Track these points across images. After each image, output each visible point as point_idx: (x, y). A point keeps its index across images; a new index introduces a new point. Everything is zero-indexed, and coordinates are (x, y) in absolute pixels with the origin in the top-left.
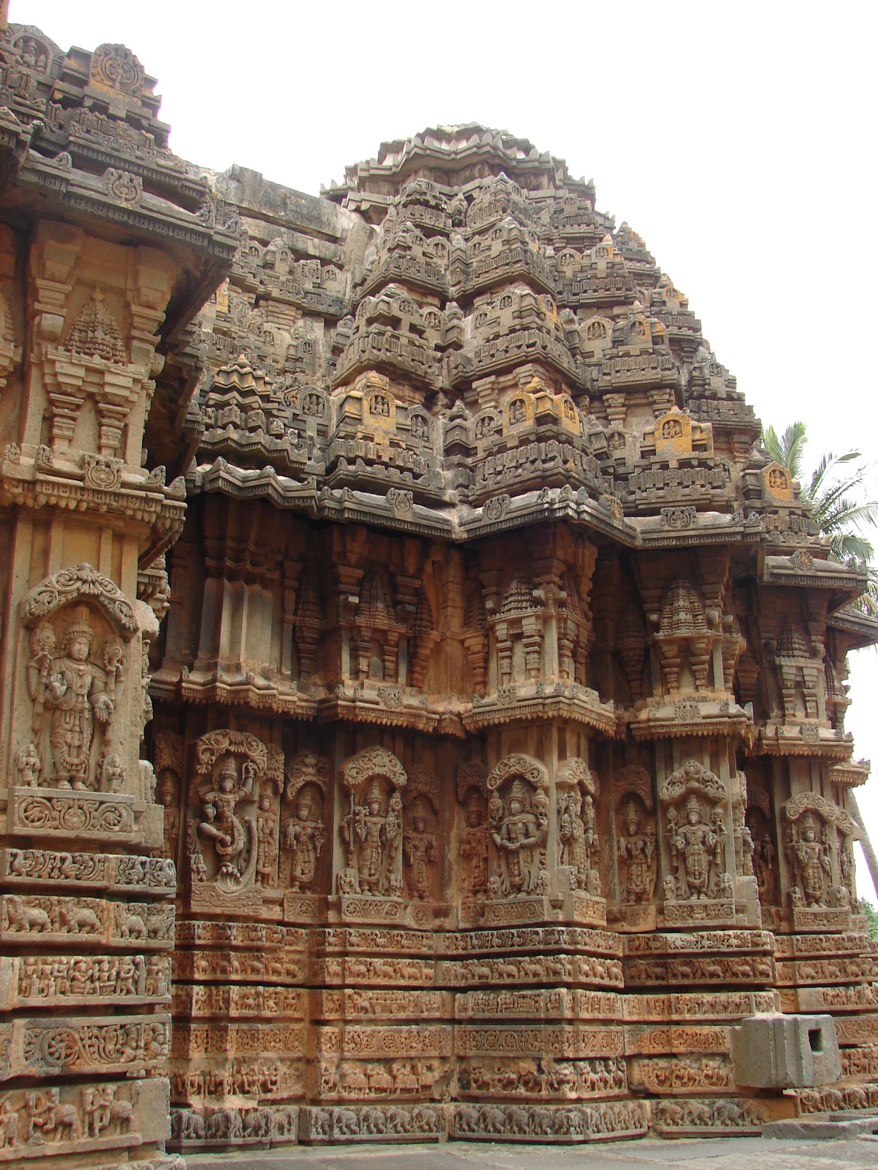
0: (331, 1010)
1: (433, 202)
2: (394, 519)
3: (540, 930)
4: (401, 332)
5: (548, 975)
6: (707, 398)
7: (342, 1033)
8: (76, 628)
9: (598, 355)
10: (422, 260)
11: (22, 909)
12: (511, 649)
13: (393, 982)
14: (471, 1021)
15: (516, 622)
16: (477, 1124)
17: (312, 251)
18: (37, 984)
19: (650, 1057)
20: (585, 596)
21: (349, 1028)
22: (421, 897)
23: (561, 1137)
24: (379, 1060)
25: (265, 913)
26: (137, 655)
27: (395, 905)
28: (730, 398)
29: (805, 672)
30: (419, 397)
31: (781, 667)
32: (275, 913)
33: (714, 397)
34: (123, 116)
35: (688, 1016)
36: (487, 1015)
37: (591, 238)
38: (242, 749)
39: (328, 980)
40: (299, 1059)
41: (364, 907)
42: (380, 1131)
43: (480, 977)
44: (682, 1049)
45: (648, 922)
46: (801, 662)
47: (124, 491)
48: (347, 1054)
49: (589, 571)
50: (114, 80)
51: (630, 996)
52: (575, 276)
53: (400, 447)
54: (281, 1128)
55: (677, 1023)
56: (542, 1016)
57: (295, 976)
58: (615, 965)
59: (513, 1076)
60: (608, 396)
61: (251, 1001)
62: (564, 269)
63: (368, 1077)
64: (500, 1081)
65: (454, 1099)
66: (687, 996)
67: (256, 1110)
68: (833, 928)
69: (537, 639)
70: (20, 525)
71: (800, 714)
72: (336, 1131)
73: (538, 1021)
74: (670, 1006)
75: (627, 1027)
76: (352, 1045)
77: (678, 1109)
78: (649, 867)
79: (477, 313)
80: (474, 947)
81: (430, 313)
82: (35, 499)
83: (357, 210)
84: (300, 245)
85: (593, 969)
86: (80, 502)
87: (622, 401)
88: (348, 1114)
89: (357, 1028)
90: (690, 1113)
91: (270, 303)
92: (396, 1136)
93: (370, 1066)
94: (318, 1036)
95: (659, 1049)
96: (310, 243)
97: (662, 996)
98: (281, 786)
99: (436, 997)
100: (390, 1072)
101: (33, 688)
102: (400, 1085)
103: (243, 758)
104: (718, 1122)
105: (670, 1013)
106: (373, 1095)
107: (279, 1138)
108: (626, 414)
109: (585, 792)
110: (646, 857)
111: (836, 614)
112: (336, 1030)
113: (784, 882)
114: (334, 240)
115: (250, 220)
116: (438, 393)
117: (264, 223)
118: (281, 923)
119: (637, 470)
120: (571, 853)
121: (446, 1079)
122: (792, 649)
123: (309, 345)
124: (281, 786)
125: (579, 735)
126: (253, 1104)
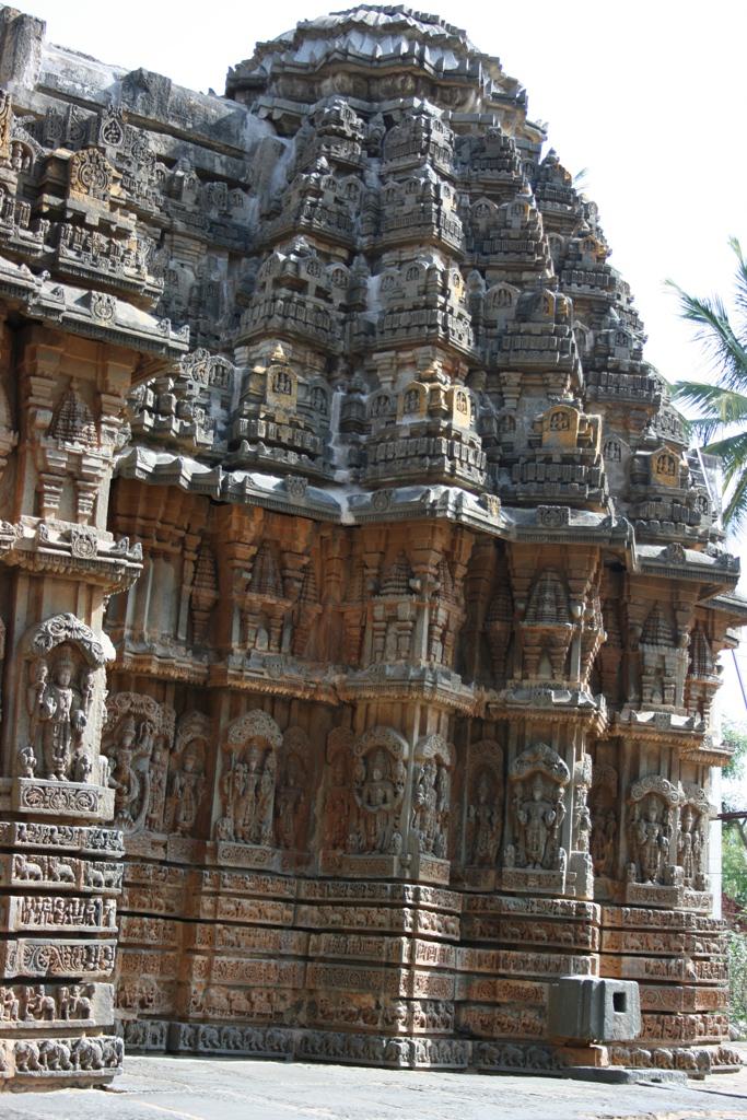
0: (202, 942)
1: (349, 134)
2: (287, 505)
3: (389, 885)
4: (308, 297)
5: (391, 925)
6: (608, 370)
7: (211, 962)
8: (63, 663)
9: (501, 326)
10: (334, 207)
11: (25, 863)
12: (386, 630)
13: (258, 921)
14: (323, 960)
15: (392, 607)
16: (320, 1047)
17: (219, 170)
18: (33, 916)
19: (477, 1003)
20: (458, 582)
21: (217, 958)
22: (287, 847)
23: (388, 1063)
24: (240, 987)
25: (150, 854)
26: (98, 679)
27: (264, 853)
28: (632, 370)
29: (667, 660)
30: (320, 363)
31: (643, 654)
32: (160, 854)
33: (617, 370)
34: (97, 224)
35: (513, 972)
36: (336, 956)
37: (510, 186)
38: (142, 711)
39: (202, 917)
40: (171, 982)
41: (238, 854)
42: (237, 1048)
43: (333, 922)
44: (505, 1000)
45: (488, 883)
46: (664, 650)
47: (99, 558)
48: (215, 981)
49: (465, 559)
50: (88, 188)
51: (464, 950)
52: (488, 231)
53: (299, 427)
54: (154, 1040)
55: (503, 976)
56: (384, 959)
57: (172, 910)
58: (453, 921)
59: (355, 1010)
60: (504, 374)
61: (137, 930)
62: (479, 221)
63: (230, 1001)
64: (343, 1013)
65: (303, 1026)
66: (514, 953)
67: (135, 1022)
68: (663, 905)
69: (411, 624)
70: (20, 580)
71: (658, 699)
72: (201, 1044)
73: (381, 964)
74: (498, 962)
75: (458, 976)
76: (219, 973)
77: (496, 1051)
78: (493, 834)
79: (383, 274)
80: (329, 896)
81: (337, 271)
82: (35, 565)
83: (269, 118)
84: (207, 165)
85: (432, 923)
86: (67, 568)
87: (518, 380)
88: (212, 1033)
89: (224, 958)
90: (506, 1055)
91: (176, 237)
92: (251, 1053)
93: (232, 992)
94: (191, 961)
95: (485, 998)
96: (217, 161)
97: (493, 952)
98: (172, 742)
99: (295, 937)
100: (249, 998)
101: (31, 709)
102: (256, 1010)
103: (141, 718)
104: (529, 1065)
105: (498, 967)
106: (233, 1017)
107: (153, 1047)
108: (520, 394)
109: (440, 764)
110: (492, 824)
111: (718, 598)
112: (206, 959)
113: (622, 857)
114: (239, 154)
115: (157, 135)
116: (337, 357)
117: (170, 138)
118: (163, 863)
119: (522, 460)
120: (423, 819)
121: (297, 1007)
122: (657, 637)
123: (214, 287)
124: (172, 742)
125: (440, 712)
126: (134, 1017)
